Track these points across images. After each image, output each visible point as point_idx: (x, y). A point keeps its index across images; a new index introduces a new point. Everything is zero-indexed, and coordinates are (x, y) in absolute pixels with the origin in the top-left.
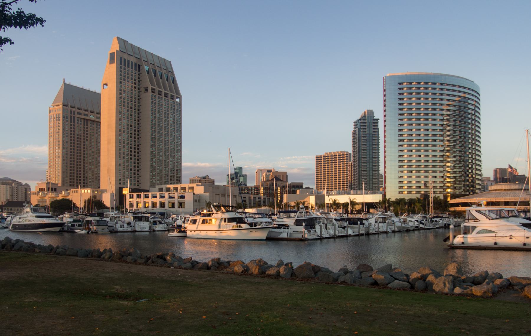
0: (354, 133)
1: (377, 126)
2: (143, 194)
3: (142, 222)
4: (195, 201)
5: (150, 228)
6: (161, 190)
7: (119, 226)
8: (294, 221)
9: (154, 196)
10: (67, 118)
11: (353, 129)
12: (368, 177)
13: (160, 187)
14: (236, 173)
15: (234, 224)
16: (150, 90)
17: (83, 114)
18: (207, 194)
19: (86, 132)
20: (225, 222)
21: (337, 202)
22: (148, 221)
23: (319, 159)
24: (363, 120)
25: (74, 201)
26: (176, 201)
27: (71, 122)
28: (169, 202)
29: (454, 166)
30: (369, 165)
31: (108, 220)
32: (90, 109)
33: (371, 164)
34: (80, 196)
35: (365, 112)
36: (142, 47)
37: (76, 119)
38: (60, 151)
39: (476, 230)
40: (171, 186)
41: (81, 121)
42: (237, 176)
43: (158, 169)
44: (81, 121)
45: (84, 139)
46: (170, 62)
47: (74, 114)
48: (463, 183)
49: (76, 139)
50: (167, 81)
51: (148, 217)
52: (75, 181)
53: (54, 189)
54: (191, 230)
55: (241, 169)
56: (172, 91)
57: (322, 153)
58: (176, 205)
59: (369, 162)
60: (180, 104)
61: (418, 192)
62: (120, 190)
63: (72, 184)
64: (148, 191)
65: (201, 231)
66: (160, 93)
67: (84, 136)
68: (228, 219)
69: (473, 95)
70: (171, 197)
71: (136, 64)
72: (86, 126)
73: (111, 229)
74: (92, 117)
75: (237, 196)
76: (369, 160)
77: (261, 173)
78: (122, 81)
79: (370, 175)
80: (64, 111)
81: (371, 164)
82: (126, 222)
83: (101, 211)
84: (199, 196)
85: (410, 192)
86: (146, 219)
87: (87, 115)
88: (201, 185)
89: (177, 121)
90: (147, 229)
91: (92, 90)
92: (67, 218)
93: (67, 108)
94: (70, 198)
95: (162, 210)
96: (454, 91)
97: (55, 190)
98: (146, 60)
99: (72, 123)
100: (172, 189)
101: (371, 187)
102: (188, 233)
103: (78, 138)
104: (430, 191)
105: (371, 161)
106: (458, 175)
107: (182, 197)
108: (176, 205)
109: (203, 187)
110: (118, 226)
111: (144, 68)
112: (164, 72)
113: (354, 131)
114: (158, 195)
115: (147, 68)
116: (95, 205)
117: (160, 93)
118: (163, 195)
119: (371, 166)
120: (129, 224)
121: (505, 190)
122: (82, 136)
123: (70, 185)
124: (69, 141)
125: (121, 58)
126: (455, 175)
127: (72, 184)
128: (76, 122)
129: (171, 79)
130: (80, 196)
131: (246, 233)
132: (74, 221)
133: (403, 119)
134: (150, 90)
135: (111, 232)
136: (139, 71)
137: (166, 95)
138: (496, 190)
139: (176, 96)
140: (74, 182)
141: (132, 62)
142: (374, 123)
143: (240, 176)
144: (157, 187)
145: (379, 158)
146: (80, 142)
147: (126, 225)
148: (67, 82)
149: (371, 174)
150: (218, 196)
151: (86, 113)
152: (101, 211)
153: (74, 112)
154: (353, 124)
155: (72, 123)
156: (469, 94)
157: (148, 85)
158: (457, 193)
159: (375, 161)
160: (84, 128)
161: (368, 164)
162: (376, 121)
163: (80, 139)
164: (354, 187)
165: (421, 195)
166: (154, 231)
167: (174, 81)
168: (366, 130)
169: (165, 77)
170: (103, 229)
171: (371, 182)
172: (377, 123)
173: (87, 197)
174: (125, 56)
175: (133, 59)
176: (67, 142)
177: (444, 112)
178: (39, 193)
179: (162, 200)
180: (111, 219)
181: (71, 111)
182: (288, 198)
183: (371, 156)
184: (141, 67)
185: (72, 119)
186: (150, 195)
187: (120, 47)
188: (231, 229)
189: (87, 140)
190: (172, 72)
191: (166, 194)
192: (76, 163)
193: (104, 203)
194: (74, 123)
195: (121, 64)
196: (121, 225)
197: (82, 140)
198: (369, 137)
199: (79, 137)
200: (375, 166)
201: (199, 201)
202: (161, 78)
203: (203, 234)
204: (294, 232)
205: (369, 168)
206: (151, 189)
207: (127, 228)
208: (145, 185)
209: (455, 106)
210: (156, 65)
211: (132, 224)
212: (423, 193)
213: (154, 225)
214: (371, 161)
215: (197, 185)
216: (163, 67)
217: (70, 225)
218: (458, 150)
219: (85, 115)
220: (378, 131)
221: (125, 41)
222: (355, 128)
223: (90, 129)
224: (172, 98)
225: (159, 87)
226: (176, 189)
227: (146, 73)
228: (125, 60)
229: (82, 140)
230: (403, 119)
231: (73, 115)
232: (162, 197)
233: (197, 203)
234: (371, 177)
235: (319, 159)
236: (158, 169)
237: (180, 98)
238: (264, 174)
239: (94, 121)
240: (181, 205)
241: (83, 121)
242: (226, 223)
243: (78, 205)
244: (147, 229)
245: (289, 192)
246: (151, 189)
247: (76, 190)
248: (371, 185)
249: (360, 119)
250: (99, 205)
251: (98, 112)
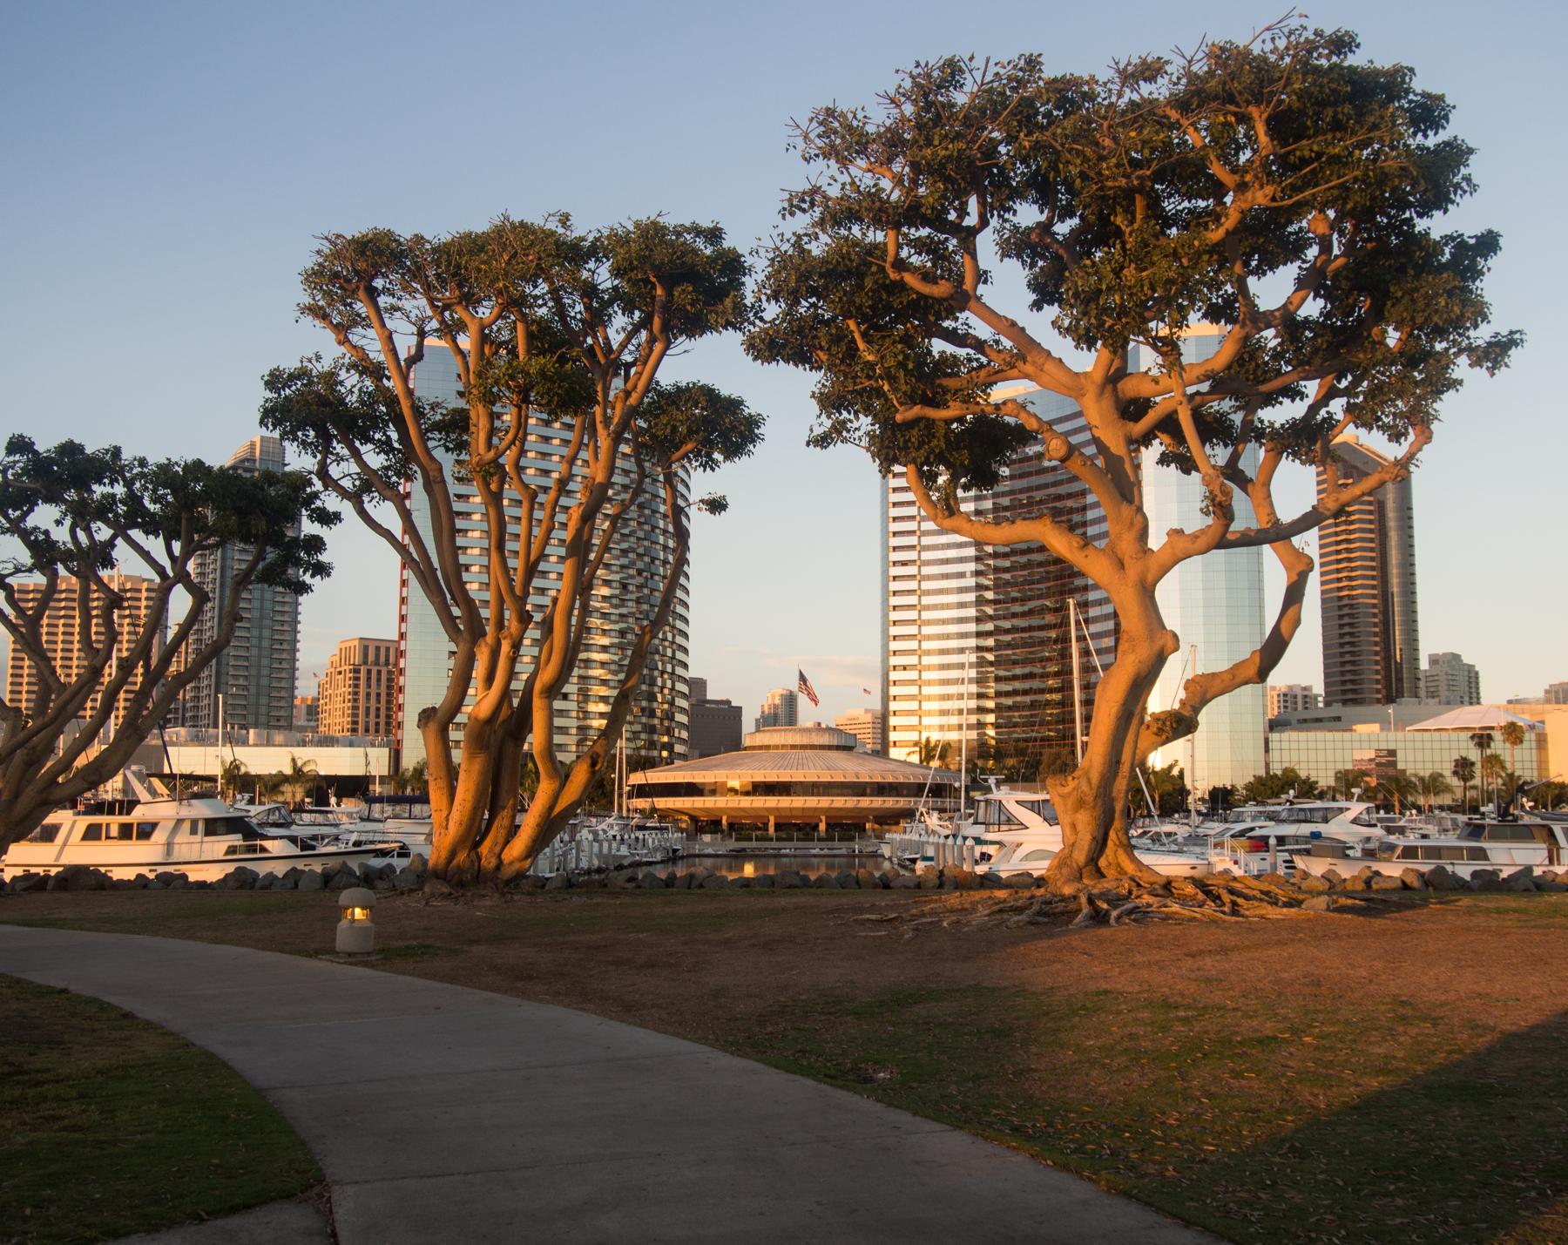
12: (253, 681)
20: (194, 831)
30: (260, 638)
33: (267, 633)
35: (253, 445)
39: (1021, 852)
59: (261, 628)
76: (261, 618)
79: (259, 676)
81: (267, 633)
101: (263, 719)
105: (267, 622)
119: (266, 643)
121: (793, 747)
133: (468, 497)
138: (768, 747)
145: (297, 613)
149: (265, 672)
159: (283, 623)
161: (255, 632)
164: (195, 717)
171: (263, 700)
183: (268, 605)
200: (281, 642)
205: (260, 647)
214: (267, 622)
230: (468, 497)
234: (264, 681)
242: (198, 838)
248: (263, 710)
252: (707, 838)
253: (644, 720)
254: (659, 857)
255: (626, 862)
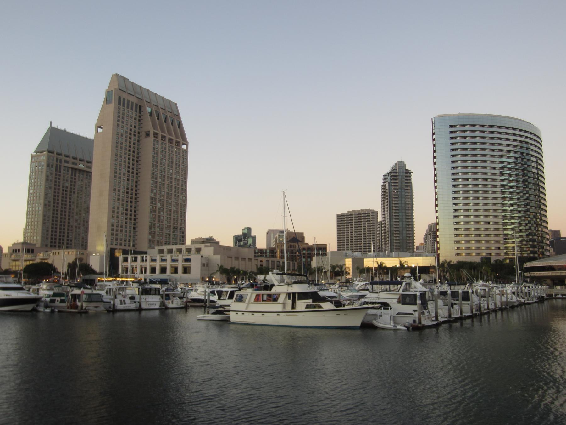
0: (383, 187)
1: (410, 180)
2: (139, 257)
3: (151, 296)
4: (203, 265)
5: (162, 304)
6: (161, 251)
7: (119, 302)
8: (397, 297)
9: (154, 258)
10: (52, 167)
11: (382, 184)
13: (161, 248)
14: (244, 235)
15: (309, 302)
16: (151, 135)
17: (71, 162)
18: (218, 257)
19: (73, 183)
21: (384, 265)
22: (159, 294)
23: (341, 218)
24: (394, 173)
25: (56, 265)
26: (180, 265)
27: (56, 171)
28: (172, 267)
29: (519, 223)
30: (402, 224)
31: (103, 293)
32: (80, 156)
34: (61, 259)
36: (144, 86)
37: (62, 168)
38: (40, 210)
40: (174, 247)
41: (68, 171)
42: (245, 238)
43: (158, 227)
44: (68, 171)
45: (71, 192)
46: (176, 104)
47: (61, 162)
48: (531, 243)
49: (61, 191)
50: (172, 125)
51: (159, 289)
52: (58, 241)
53: (30, 251)
54: (237, 312)
55: (249, 229)
56: (177, 137)
57: (345, 212)
58: (180, 270)
60: (186, 152)
61: (478, 254)
62: (112, 252)
63: (53, 244)
64: (146, 253)
65: (253, 312)
66: (163, 138)
67: (71, 188)
68: (299, 294)
69: (535, 140)
70: (173, 260)
71: (136, 105)
72: (73, 177)
73: (108, 305)
74: (81, 166)
75: (253, 260)
77: (272, 235)
78: (120, 123)
80: (49, 158)
82: (128, 297)
83: (88, 277)
84: (208, 259)
85: (469, 254)
86: (156, 292)
87: (76, 164)
88: (210, 246)
89: (182, 171)
90: (157, 306)
91: (83, 135)
92: (44, 290)
93: (52, 155)
94: (50, 261)
95: (163, 276)
96: (515, 135)
97: (33, 251)
98: (149, 101)
99: (58, 173)
100: (174, 250)
102: (232, 314)
103: (63, 190)
104: (493, 251)
106: (525, 234)
107: (188, 260)
108: (180, 270)
109: (212, 248)
110: (117, 302)
111: (146, 110)
112: (169, 115)
113: (383, 186)
114: (158, 258)
115: (149, 110)
116: (81, 271)
117: (163, 138)
118: (163, 258)
119: (404, 226)
120: (132, 298)
122: (69, 188)
123: (51, 246)
124: (54, 180)
125: (120, 98)
126: (521, 234)
127: (53, 244)
128: (62, 171)
129: (176, 123)
130: (61, 259)
131: (324, 318)
132: (55, 295)
134: (151, 135)
135: (109, 311)
136: (140, 112)
137: (171, 140)
139: (182, 142)
140: (55, 243)
141: (132, 103)
142: (406, 176)
143: (248, 238)
144: (157, 248)
146: (66, 194)
147: (128, 301)
148: (54, 125)
150: (230, 259)
151: (75, 161)
152: (88, 277)
153: (61, 160)
154: (382, 178)
155: (58, 173)
156: (531, 139)
157: (147, 131)
158: (525, 255)
160: (72, 178)
162: (408, 175)
163: (66, 191)
165: (482, 258)
166: (167, 308)
167: (180, 125)
168: (398, 183)
169: (170, 121)
170: (96, 307)
172: (410, 176)
173: (71, 259)
174: (124, 96)
175: (133, 99)
176: (51, 181)
177: (504, 160)
178: (11, 255)
179: (163, 264)
180: (107, 292)
181: (57, 159)
182: (318, 262)
184: (142, 109)
185: (58, 168)
186: (148, 258)
187: (119, 85)
188: (304, 309)
189: (74, 193)
190: (178, 116)
191: (168, 257)
192: (58, 226)
193: (92, 267)
194: (60, 172)
195: (119, 104)
196: (121, 301)
197: (68, 193)
198: (401, 192)
199: (65, 189)
200: (409, 225)
201: (208, 265)
202: (165, 122)
203: (258, 319)
204: (398, 314)
206: (149, 251)
207: (130, 305)
208: (143, 245)
209: (515, 152)
210: (160, 106)
211: (137, 298)
212: (484, 254)
213: (166, 299)
215: (206, 246)
216: (167, 109)
217: (48, 299)
218: (523, 203)
219: (73, 163)
220: (411, 186)
221: (125, 79)
222: (384, 182)
223: (79, 180)
224: (178, 143)
225: (163, 131)
226: (180, 251)
227: (149, 115)
228: (124, 99)
229: (68, 193)
231: (59, 163)
232: (163, 260)
233: (205, 268)
235: (341, 218)
236: (158, 227)
237: (186, 144)
238: (277, 236)
239: (83, 171)
240: (186, 270)
241: (70, 170)
243: (60, 269)
244: (157, 306)
245: (318, 255)
246: (149, 251)
247: (57, 251)
249: (390, 173)
250: (86, 269)
251: (89, 160)
252: (558, 288)
253: (531, 249)
254: (535, 300)
255: (516, 304)
